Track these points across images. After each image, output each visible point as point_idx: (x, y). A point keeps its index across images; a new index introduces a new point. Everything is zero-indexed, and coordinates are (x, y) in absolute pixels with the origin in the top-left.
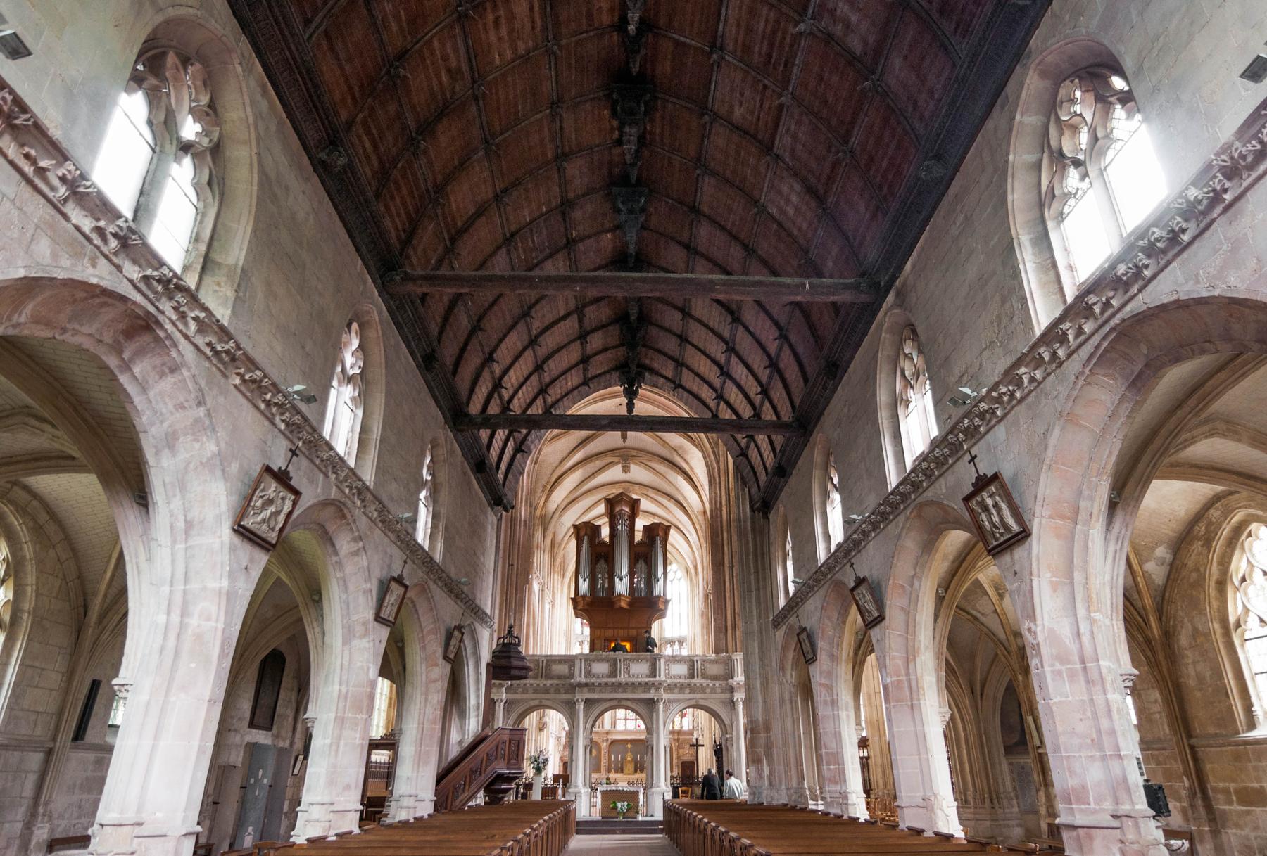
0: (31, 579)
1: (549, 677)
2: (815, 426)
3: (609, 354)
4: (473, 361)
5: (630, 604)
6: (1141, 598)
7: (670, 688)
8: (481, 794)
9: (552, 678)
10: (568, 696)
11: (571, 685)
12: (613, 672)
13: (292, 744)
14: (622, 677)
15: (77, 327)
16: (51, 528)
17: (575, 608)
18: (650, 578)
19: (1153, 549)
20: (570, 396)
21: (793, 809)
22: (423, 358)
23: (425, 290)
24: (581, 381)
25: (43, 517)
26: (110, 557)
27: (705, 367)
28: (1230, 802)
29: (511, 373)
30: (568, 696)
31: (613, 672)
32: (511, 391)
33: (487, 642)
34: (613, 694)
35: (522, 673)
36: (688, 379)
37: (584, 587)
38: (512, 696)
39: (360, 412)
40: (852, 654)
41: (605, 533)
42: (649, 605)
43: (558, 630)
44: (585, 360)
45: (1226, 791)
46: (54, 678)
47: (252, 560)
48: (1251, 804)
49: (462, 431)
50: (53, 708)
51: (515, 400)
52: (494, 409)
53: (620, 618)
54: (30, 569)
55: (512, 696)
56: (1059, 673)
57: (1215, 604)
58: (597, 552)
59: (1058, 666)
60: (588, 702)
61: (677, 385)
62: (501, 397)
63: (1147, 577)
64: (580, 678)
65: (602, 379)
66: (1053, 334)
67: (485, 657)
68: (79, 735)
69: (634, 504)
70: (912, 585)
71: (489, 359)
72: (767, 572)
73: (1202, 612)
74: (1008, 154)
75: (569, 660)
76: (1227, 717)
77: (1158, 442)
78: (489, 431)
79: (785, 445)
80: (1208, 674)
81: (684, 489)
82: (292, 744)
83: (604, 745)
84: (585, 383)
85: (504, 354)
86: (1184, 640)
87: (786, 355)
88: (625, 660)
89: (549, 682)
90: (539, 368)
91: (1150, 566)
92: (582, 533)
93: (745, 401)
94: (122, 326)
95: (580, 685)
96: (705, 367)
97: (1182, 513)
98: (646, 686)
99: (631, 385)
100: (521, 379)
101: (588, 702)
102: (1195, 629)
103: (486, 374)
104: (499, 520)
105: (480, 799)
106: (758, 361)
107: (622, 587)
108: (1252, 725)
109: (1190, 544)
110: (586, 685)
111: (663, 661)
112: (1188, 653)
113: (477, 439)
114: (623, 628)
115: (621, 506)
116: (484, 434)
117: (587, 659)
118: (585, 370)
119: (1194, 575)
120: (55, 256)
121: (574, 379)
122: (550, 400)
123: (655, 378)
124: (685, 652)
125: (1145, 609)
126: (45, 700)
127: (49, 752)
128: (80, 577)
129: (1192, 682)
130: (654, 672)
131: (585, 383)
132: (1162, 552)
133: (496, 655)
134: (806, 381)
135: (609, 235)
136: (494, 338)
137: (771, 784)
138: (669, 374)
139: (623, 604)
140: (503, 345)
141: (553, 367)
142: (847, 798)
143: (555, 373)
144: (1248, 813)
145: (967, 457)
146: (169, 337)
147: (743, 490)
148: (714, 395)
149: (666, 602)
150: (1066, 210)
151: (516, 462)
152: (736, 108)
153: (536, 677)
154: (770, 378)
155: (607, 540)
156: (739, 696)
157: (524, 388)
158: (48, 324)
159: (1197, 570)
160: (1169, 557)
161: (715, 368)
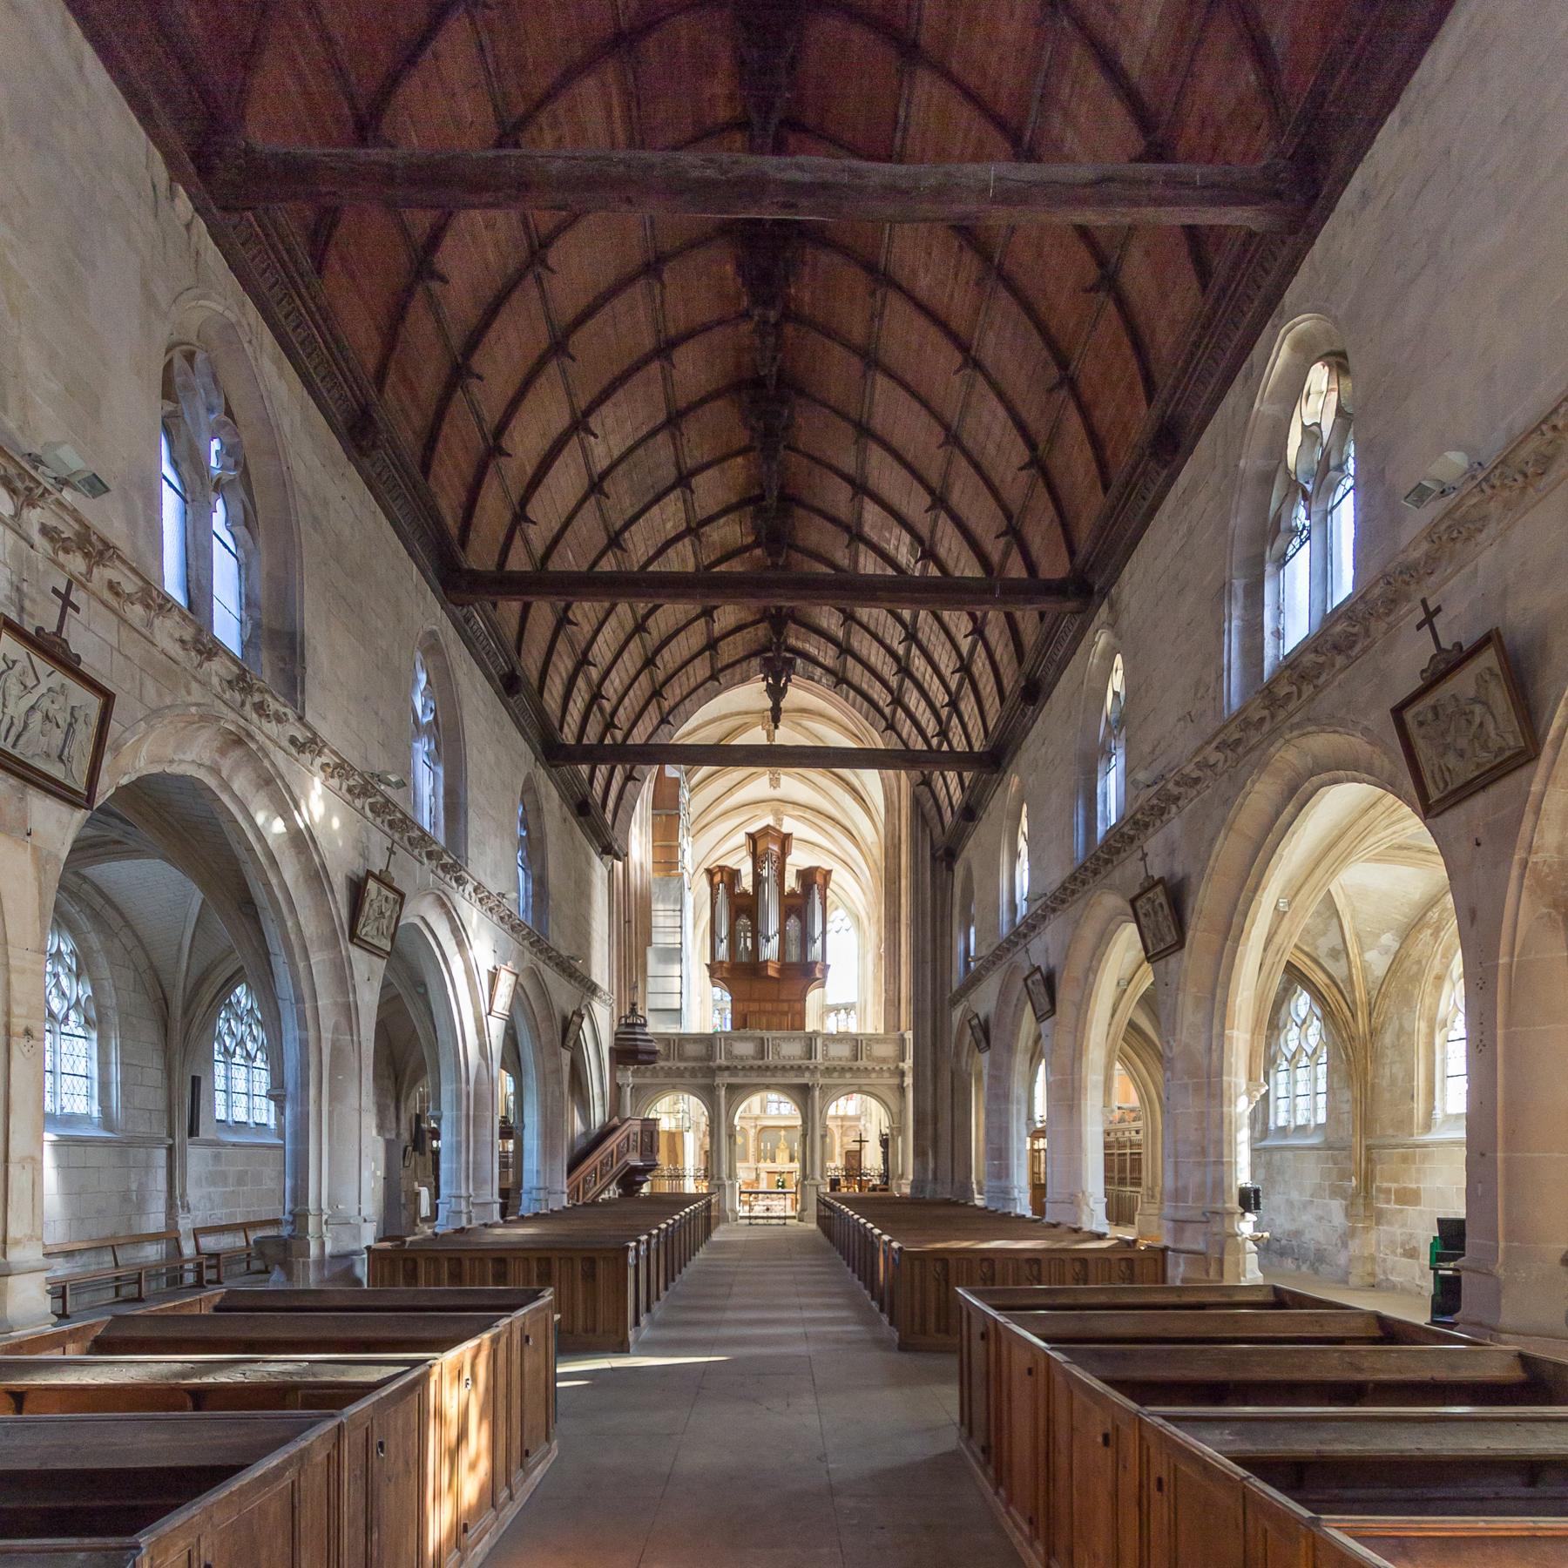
0: (105, 972)
1: (682, 1058)
2: (1010, 763)
3: (748, 634)
4: (564, 663)
5: (780, 971)
6: (1353, 991)
7: (829, 1071)
8: (613, 1186)
9: (686, 1060)
10: (708, 1081)
11: (709, 1068)
12: (761, 1053)
13: (398, 1135)
14: (771, 1060)
15: (182, 757)
16: (109, 913)
17: (711, 976)
18: (805, 938)
19: (1379, 936)
20: (694, 697)
21: (955, 1204)
22: (501, 678)
23: (361, 153)
24: (708, 674)
25: (98, 902)
26: (180, 949)
27: (876, 656)
28: (1388, 1202)
29: (613, 674)
30: (708, 1081)
31: (761, 1053)
32: (614, 699)
33: (602, 1020)
34: (762, 1074)
35: (651, 1058)
36: (856, 672)
37: (723, 949)
38: (639, 1081)
39: (441, 771)
40: (1030, 1043)
41: (747, 883)
42: (803, 972)
43: (696, 1003)
44: (712, 645)
45: (1388, 1191)
46: (154, 1075)
47: (372, 971)
48: (1405, 1203)
49: (556, 766)
50: (162, 1105)
51: (621, 710)
52: (591, 737)
53: (766, 983)
54: (101, 960)
55: (639, 1081)
56: (1185, 1086)
57: (1427, 1001)
58: (739, 906)
59: (1186, 1080)
60: (731, 1088)
61: (840, 680)
62: (601, 710)
63: (1365, 969)
64: (721, 1061)
65: (738, 669)
66: (1304, 668)
67: (606, 1041)
68: (193, 1131)
69: (785, 840)
70: (1087, 977)
71: (583, 661)
72: (947, 939)
73: (1412, 1010)
74: (1240, 458)
75: (708, 1040)
76: (1405, 1123)
77: (1342, 845)
78: (585, 741)
79: (975, 782)
80: (1401, 1076)
81: (845, 836)
82: (398, 1135)
83: (752, 1133)
84: (713, 677)
85: (602, 651)
86: (1388, 1038)
87: (980, 665)
88: (774, 1039)
89: (682, 1065)
90: (649, 662)
91: (1371, 956)
92: (717, 878)
93: (928, 711)
94: (216, 744)
95: (720, 1068)
96: (876, 656)
97: (1417, 897)
98: (800, 1070)
99: (777, 680)
100: (627, 681)
101: (731, 1088)
102: (1401, 1027)
103: (581, 682)
104: (611, 872)
105: (613, 1192)
106: (947, 662)
107: (770, 951)
108: (1428, 1127)
109: (1419, 931)
110: (727, 1068)
111: (819, 1042)
112: (1389, 1052)
113: (577, 774)
114: (771, 1001)
115: (768, 846)
116: (584, 769)
117: (727, 1037)
118: (710, 630)
119: (1415, 968)
120: (160, 695)
121: (700, 669)
122: (666, 705)
123: (810, 668)
124: (853, 1028)
125: (1354, 1002)
126: (157, 1100)
127: (170, 1149)
128: (152, 966)
129: (1385, 1083)
130: (810, 1053)
131: (713, 677)
132: (1389, 940)
133: (618, 1037)
134: (1002, 700)
135: (740, 460)
136: (587, 629)
137: (935, 1178)
138: (829, 662)
139: (771, 972)
140: (600, 638)
141: (670, 658)
142: (1007, 1193)
143: (671, 667)
144: (1401, 1211)
145: (1140, 854)
146: (261, 748)
147: (923, 831)
148: (889, 699)
149: (826, 968)
150: (1290, 552)
151: (627, 794)
152: (921, 273)
153: (667, 1059)
154: (960, 685)
155: (750, 890)
156: (909, 1080)
157: (631, 693)
158: (160, 761)
159: (1419, 962)
160: (1396, 946)
161: (889, 660)
